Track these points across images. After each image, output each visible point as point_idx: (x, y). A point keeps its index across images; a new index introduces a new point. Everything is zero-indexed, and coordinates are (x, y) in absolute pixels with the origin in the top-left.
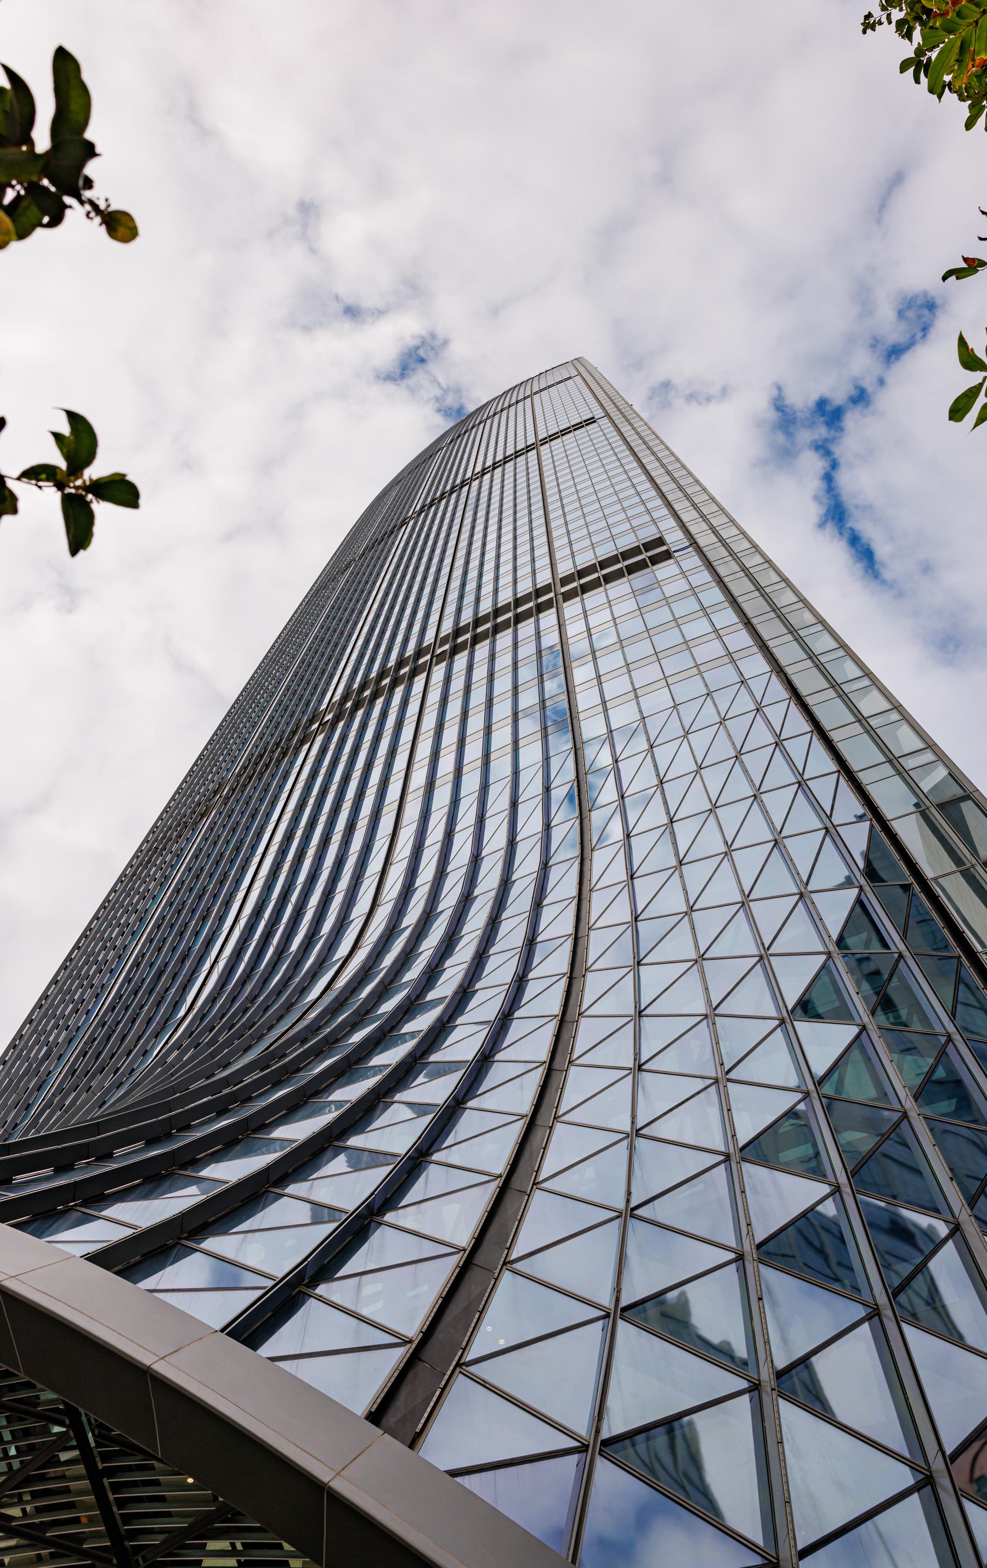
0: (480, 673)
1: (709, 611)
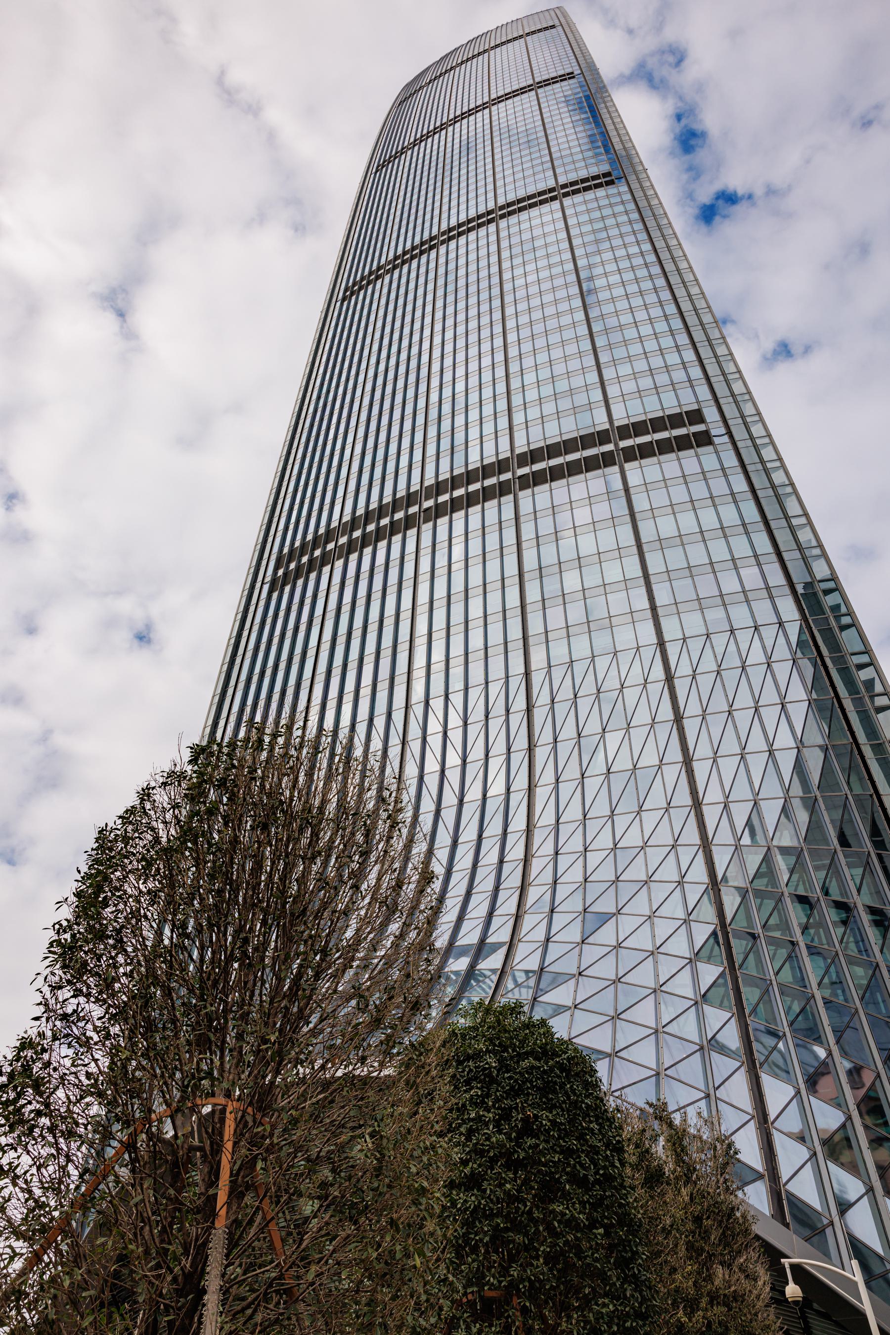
1: (664, 351)
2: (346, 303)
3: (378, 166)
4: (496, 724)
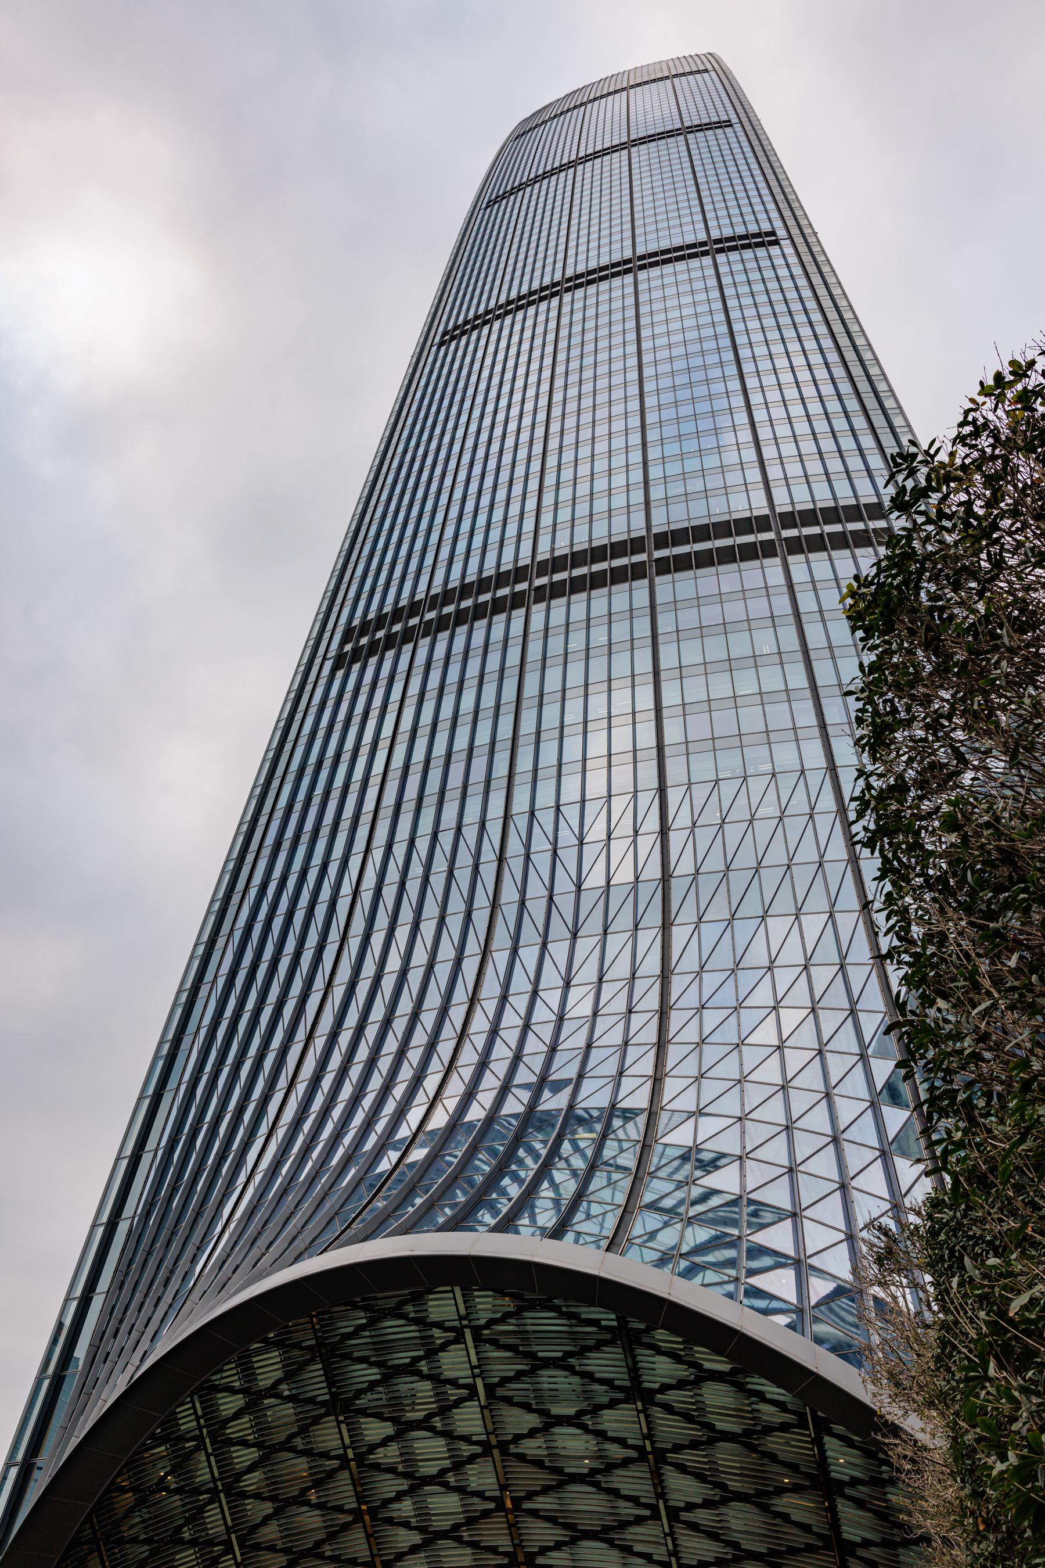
0: (517, 327)
2: (443, 349)
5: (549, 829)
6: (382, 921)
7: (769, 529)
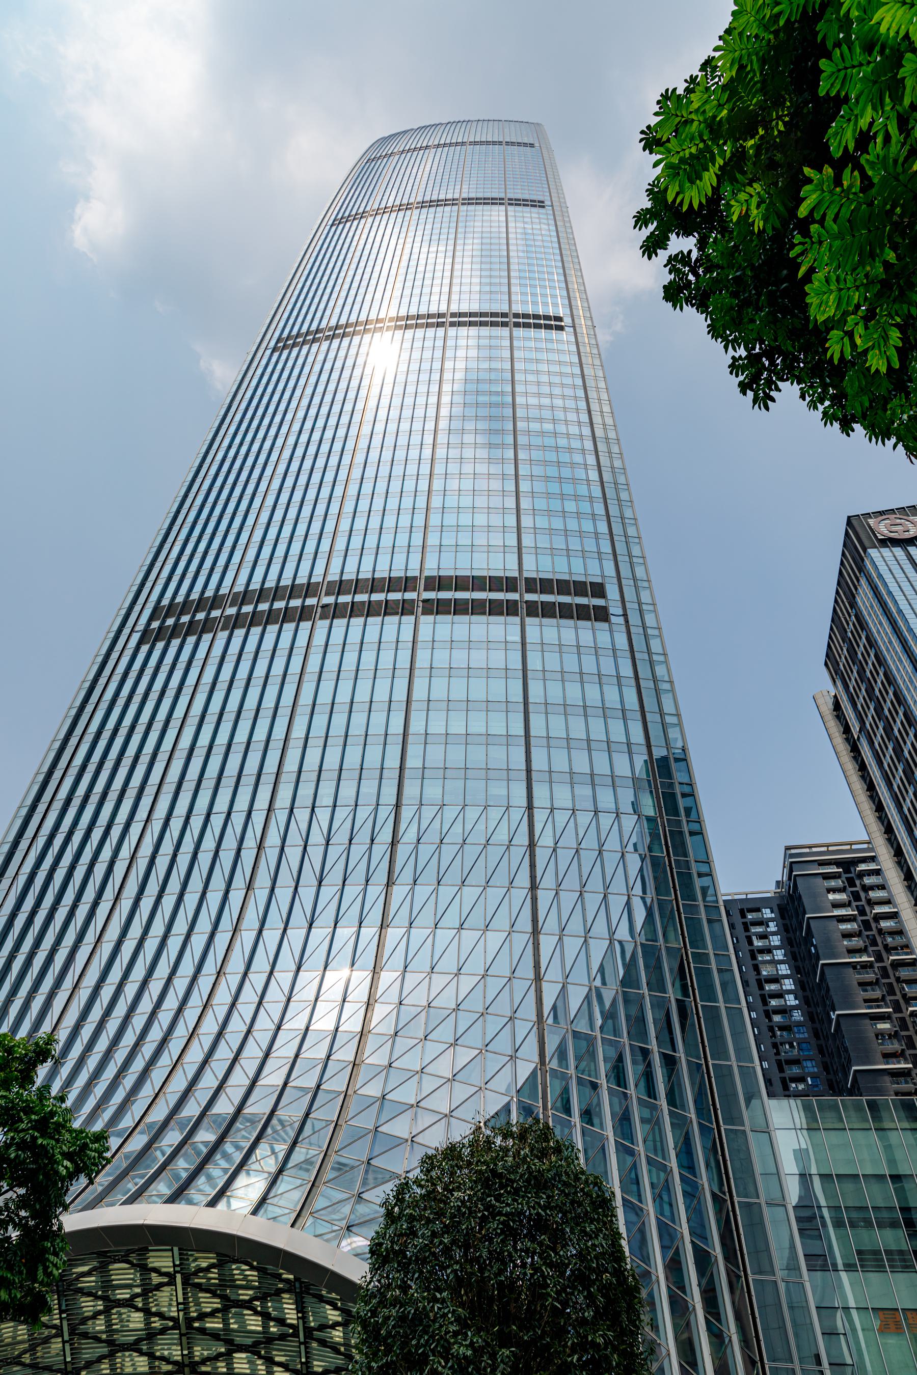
3: (334, 220)
4: (358, 850)
5: (304, 827)
6: (153, 888)
7: (515, 590)
